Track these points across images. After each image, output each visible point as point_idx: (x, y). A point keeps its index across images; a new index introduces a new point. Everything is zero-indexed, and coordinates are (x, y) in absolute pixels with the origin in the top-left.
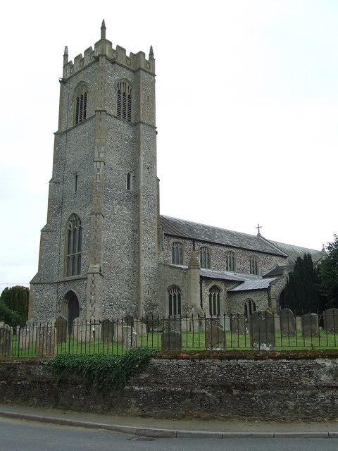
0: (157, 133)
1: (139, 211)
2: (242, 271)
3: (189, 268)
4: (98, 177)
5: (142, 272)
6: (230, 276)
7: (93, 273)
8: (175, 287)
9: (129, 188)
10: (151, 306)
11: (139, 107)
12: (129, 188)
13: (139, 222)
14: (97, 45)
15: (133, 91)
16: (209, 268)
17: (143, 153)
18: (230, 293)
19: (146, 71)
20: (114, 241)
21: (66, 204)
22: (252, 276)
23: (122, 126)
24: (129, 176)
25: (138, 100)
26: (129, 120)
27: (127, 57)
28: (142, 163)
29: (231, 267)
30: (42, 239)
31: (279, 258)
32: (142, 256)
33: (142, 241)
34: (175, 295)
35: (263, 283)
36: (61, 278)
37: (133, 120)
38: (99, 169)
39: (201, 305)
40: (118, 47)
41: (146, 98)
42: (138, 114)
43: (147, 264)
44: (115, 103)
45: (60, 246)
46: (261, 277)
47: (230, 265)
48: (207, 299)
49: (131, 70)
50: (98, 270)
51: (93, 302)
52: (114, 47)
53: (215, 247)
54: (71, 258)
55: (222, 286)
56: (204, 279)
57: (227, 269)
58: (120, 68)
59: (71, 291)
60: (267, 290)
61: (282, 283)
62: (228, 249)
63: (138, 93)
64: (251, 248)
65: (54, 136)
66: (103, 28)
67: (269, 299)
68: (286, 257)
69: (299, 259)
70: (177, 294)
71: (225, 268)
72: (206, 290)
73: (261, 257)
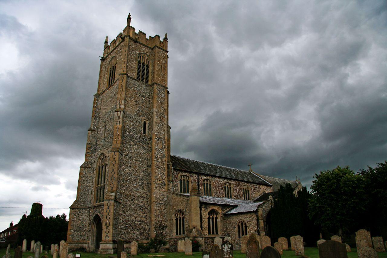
0: (168, 93)
1: (151, 151)
2: (237, 197)
3: (191, 196)
4: (118, 123)
5: (154, 199)
6: (227, 202)
7: (109, 200)
8: (180, 211)
9: (145, 132)
10: (161, 227)
11: (154, 73)
12: (145, 132)
13: (151, 160)
14: (124, 31)
15: (151, 62)
16: (211, 195)
17: (156, 105)
18: (226, 216)
19: (160, 49)
20: (130, 174)
21: (98, 147)
22: (246, 201)
23: (141, 86)
24: (145, 124)
25: (153, 69)
26: (147, 82)
27: (146, 39)
28: (155, 114)
29: (228, 195)
30: (80, 173)
31: (265, 187)
32: (154, 186)
33: (154, 174)
34: (180, 218)
35: (252, 206)
36: (92, 204)
37: (150, 83)
38: (119, 117)
39: (201, 226)
40: (140, 32)
41: (160, 67)
42: (153, 78)
43: (158, 192)
44: (136, 70)
45: (93, 179)
46: (253, 202)
47: (228, 193)
48: (207, 220)
49: (150, 48)
50: (113, 198)
51: (108, 225)
52: (137, 32)
53: (216, 179)
54: (100, 183)
55: (220, 210)
56: (203, 204)
57: (226, 196)
58: (141, 46)
59: (97, 215)
60: (256, 212)
61: (268, 205)
62: (226, 181)
63: (154, 64)
64: (245, 179)
65: (93, 97)
66: (129, 19)
67: (258, 220)
68: (271, 186)
69: (281, 186)
70: (182, 217)
71: (224, 195)
72: (205, 214)
73: (252, 187)
